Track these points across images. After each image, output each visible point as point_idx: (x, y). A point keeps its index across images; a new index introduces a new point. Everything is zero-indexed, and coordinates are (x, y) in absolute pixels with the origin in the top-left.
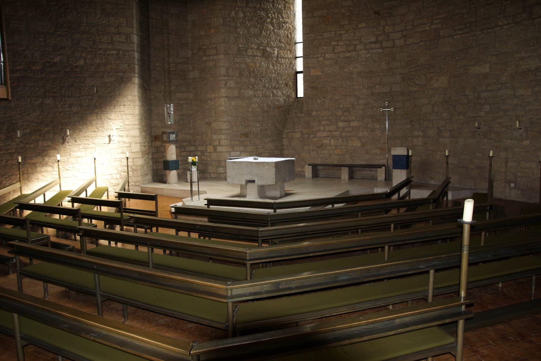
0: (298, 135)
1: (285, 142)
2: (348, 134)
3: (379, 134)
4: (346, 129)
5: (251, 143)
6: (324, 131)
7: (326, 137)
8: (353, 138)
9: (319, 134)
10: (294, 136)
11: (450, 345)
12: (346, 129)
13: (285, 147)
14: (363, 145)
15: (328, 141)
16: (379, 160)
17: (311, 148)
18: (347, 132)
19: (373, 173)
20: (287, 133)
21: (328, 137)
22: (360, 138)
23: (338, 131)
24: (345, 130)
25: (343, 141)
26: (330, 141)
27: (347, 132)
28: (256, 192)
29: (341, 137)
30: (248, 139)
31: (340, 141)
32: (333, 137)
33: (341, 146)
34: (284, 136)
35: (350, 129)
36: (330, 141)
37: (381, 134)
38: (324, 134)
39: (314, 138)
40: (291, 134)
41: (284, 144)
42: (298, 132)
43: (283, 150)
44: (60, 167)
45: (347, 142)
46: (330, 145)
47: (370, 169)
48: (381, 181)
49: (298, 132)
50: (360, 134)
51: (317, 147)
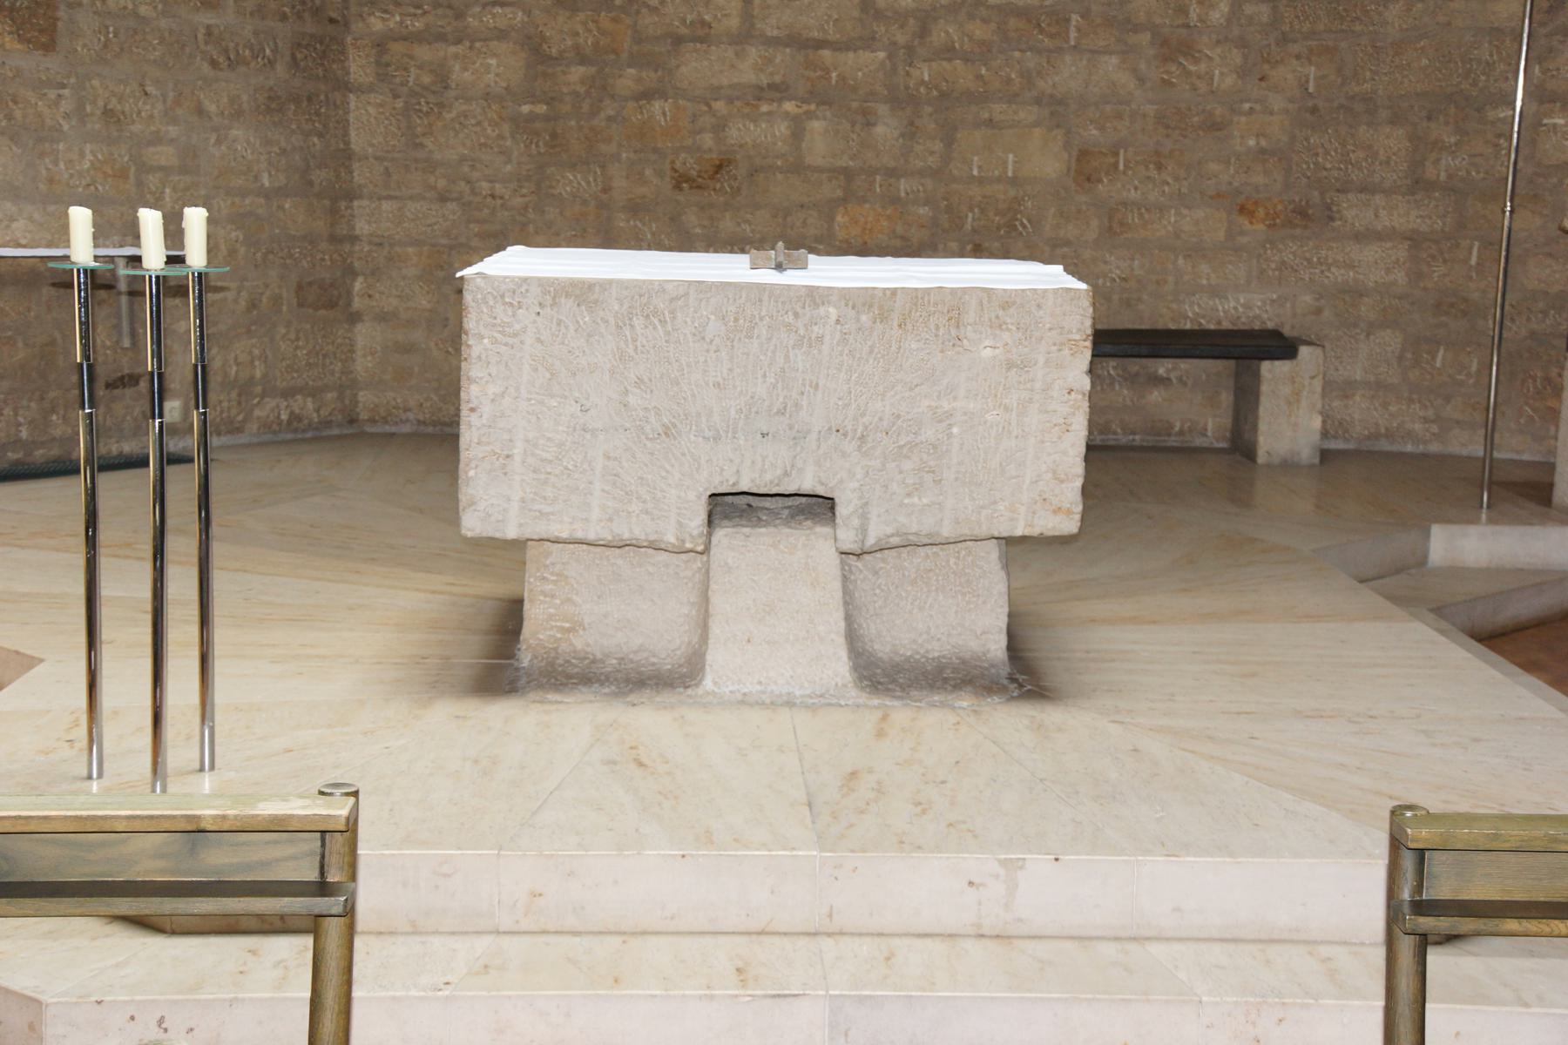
0: (498, 67)
1: (368, 122)
2: (962, 75)
3: (1226, 81)
4: (944, 32)
5: (80, 114)
6: (743, 38)
7: (761, 93)
8: (998, 109)
9: (694, 68)
10: (459, 75)
11: (71, 911)
12: (944, 32)
13: (361, 175)
14: (1087, 168)
15: (782, 128)
16: (1215, 292)
17: (620, 183)
18: (948, 52)
19: (1156, 396)
20: (380, 45)
21: (779, 91)
22: (1056, 109)
23: (868, 42)
24: (938, 36)
25: (911, 132)
26: (797, 134)
27: (948, 52)
28: (526, 623)
29: (903, 100)
30: (51, 64)
31: (886, 129)
32: (820, 97)
33: (892, 173)
34: (359, 67)
35: (980, 31)
36: (797, 134)
37: (1243, 73)
38: (747, 69)
39: (646, 96)
40: (423, 53)
41: (357, 141)
42: (501, 35)
43: (351, 195)
44: (714, 540)
45: (949, 142)
46: (798, 168)
47: (1135, 365)
48: (1288, 466)
49: (501, 35)
50: (1068, 75)
51: (681, 181)
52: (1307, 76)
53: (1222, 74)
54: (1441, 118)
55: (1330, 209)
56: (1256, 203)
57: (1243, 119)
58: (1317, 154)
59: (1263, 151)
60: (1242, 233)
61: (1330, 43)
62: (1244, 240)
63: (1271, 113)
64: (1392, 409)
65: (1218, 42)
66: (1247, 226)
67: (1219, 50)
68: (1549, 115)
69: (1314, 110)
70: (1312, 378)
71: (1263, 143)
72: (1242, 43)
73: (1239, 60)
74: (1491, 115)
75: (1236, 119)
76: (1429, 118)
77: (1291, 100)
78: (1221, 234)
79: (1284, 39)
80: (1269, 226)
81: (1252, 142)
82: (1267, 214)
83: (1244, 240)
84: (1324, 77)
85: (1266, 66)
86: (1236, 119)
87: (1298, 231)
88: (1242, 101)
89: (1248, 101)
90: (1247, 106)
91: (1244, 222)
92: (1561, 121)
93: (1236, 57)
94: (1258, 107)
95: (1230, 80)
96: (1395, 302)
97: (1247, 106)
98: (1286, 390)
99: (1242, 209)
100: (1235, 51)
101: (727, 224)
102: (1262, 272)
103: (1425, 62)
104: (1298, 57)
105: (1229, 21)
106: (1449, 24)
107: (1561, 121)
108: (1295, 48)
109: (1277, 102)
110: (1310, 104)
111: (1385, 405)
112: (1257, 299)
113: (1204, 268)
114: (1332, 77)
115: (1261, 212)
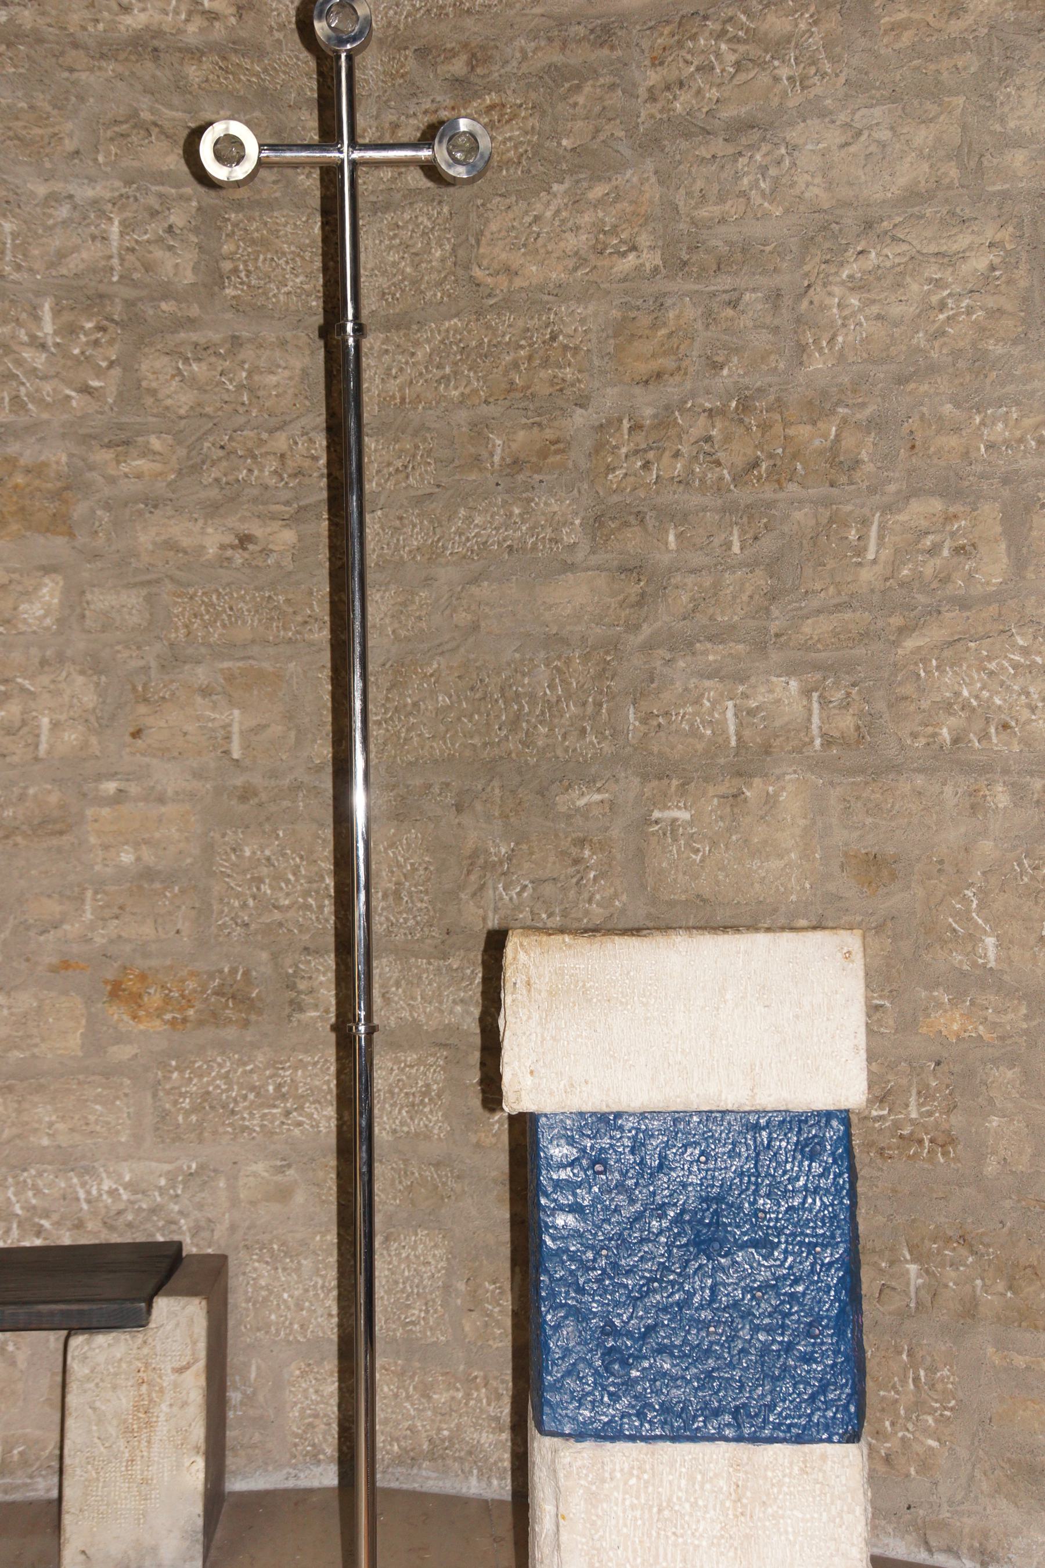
52: (226, 727)
53: (55, 725)
54: (479, 807)
55: (292, 987)
56: (143, 977)
57: (105, 811)
58: (260, 880)
59: (148, 874)
60: (120, 1039)
61: (267, 666)
62: (123, 1053)
63: (161, 800)
64: (440, 1398)
65: (44, 663)
66: (127, 1024)
67: (45, 680)
68: (662, 801)
69: (246, 794)
70: (180, 1370)
71: (148, 856)
72: (95, 666)
73: (90, 699)
74: (563, 802)
75: (90, 812)
76: (459, 808)
77: (198, 775)
78: (74, 1042)
79: (174, 659)
80: (173, 1023)
81: (127, 857)
82: (167, 1000)
83: (123, 1053)
84: (261, 728)
85: (142, 709)
86: (90, 812)
87: (230, 1033)
88: (100, 777)
89: (112, 776)
90: (110, 787)
91: (118, 1014)
92: (684, 815)
93: (82, 690)
94: (133, 789)
95: (71, 737)
96: (429, 1173)
97: (110, 787)
98: (124, 1401)
99: (116, 991)
100: (80, 680)
101: (517, 1269)
102: (164, 1116)
103: (443, 700)
104: (206, 692)
105: (61, 621)
106: (475, 627)
107: (684, 815)
108: (201, 675)
109: (170, 778)
110: (239, 781)
111: (426, 1391)
112: (156, 1171)
113: (43, 1112)
114: (277, 729)
115: (154, 998)
